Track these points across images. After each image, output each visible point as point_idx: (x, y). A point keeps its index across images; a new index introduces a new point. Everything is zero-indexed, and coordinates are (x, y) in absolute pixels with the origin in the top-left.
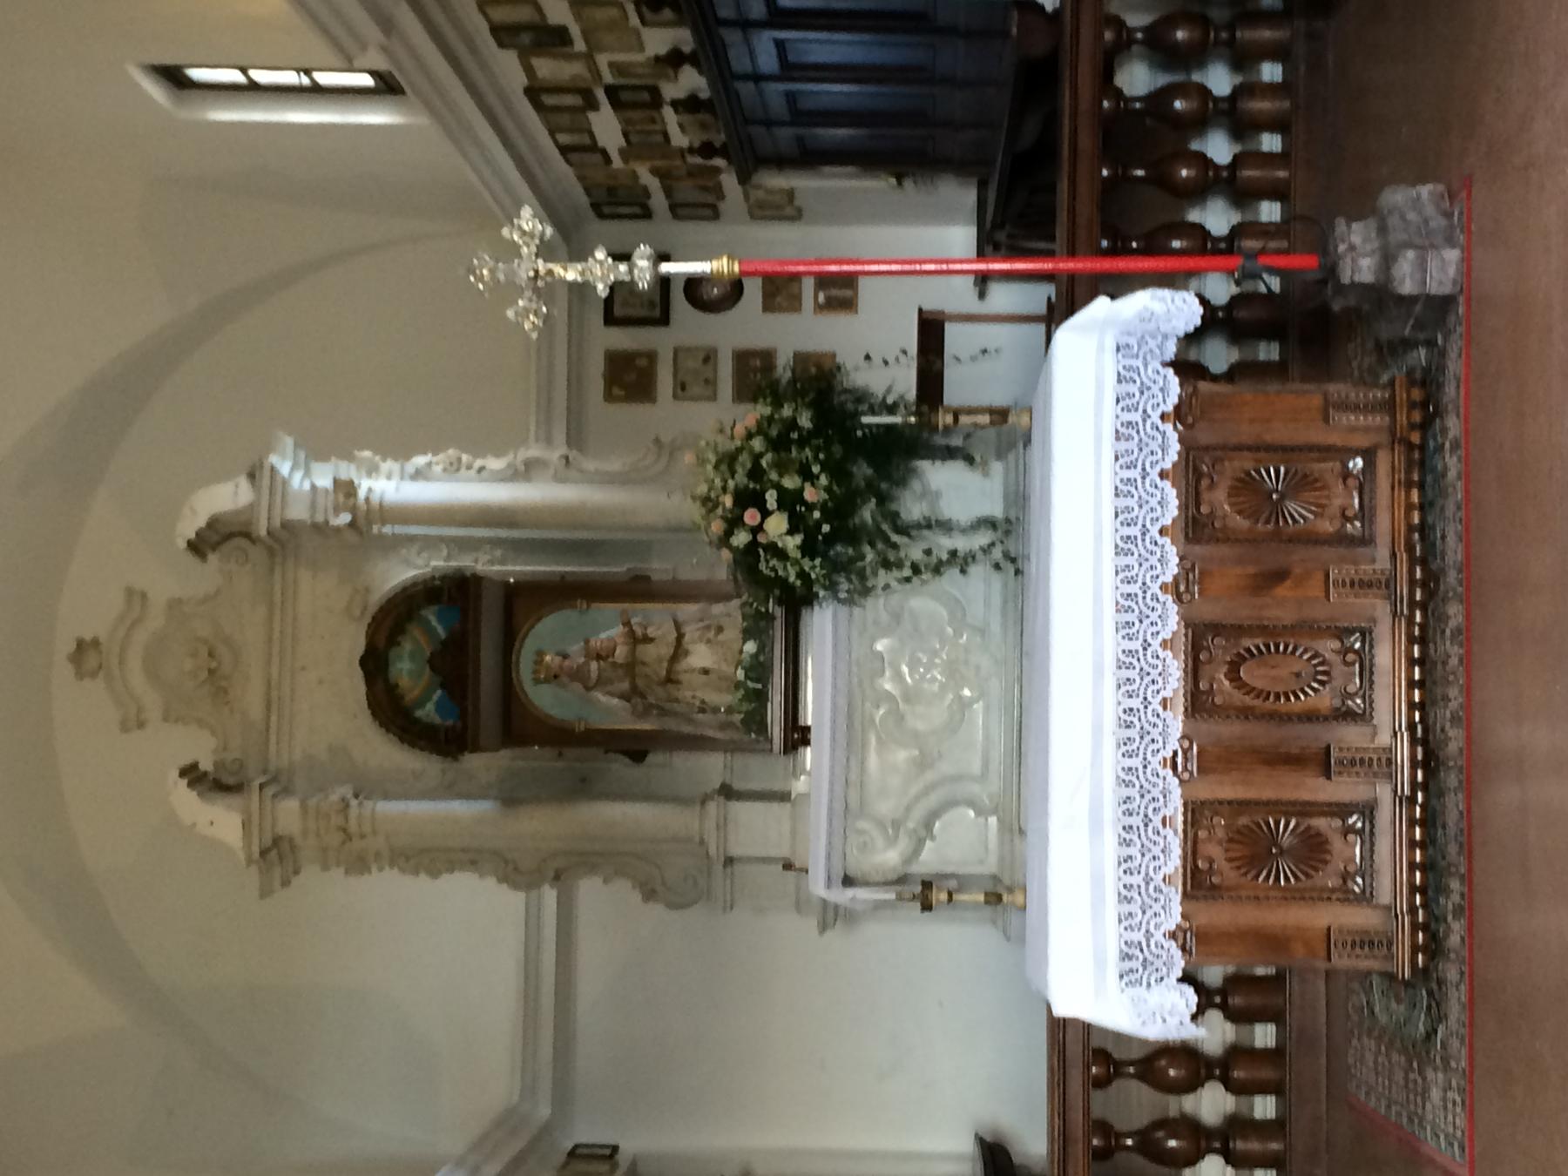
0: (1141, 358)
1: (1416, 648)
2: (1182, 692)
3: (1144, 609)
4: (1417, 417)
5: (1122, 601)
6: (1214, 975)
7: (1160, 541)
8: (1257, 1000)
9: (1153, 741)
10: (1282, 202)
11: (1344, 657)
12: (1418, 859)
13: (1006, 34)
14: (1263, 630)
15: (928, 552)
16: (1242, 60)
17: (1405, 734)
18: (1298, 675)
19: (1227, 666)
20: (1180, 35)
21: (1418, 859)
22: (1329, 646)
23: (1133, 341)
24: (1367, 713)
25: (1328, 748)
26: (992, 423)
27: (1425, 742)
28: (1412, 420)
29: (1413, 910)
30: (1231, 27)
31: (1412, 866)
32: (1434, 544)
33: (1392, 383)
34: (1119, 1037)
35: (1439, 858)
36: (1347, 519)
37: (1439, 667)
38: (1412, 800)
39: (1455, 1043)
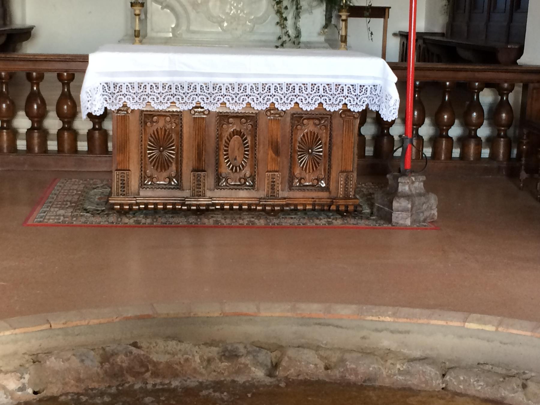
0: (370, 95)
1: (246, 207)
2: (228, 111)
3: (263, 96)
4: (342, 208)
5: (267, 86)
6: (108, 125)
7: (292, 103)
8: (97, 143)
9: (208, 98)
10: (431, 157)
11: (243, 178)
12: (159, 207)
13: (508, 43)
14: (254, 145)
15: (286, 8)
16: (491, 141)
17: (211, 202)
18: (235, 159)
19: (239, 130)
20: (504, 115)
21: (159, 207)
22: (247, 172)
23: (378, 92)
24: (219, 187)
25: (204, 171)
26: (342, 36)
27: (207, 210)
28: (340, 206)
29: (138, 204)
30: (505, 136)
31: (156, 204)
32: (289, 215)
33: (356, 198)
34: (80, 87)
35: (160, 215)
36: (300, 181)
37: (238, 216)
38: (183, 204)
39: (83, 219)
